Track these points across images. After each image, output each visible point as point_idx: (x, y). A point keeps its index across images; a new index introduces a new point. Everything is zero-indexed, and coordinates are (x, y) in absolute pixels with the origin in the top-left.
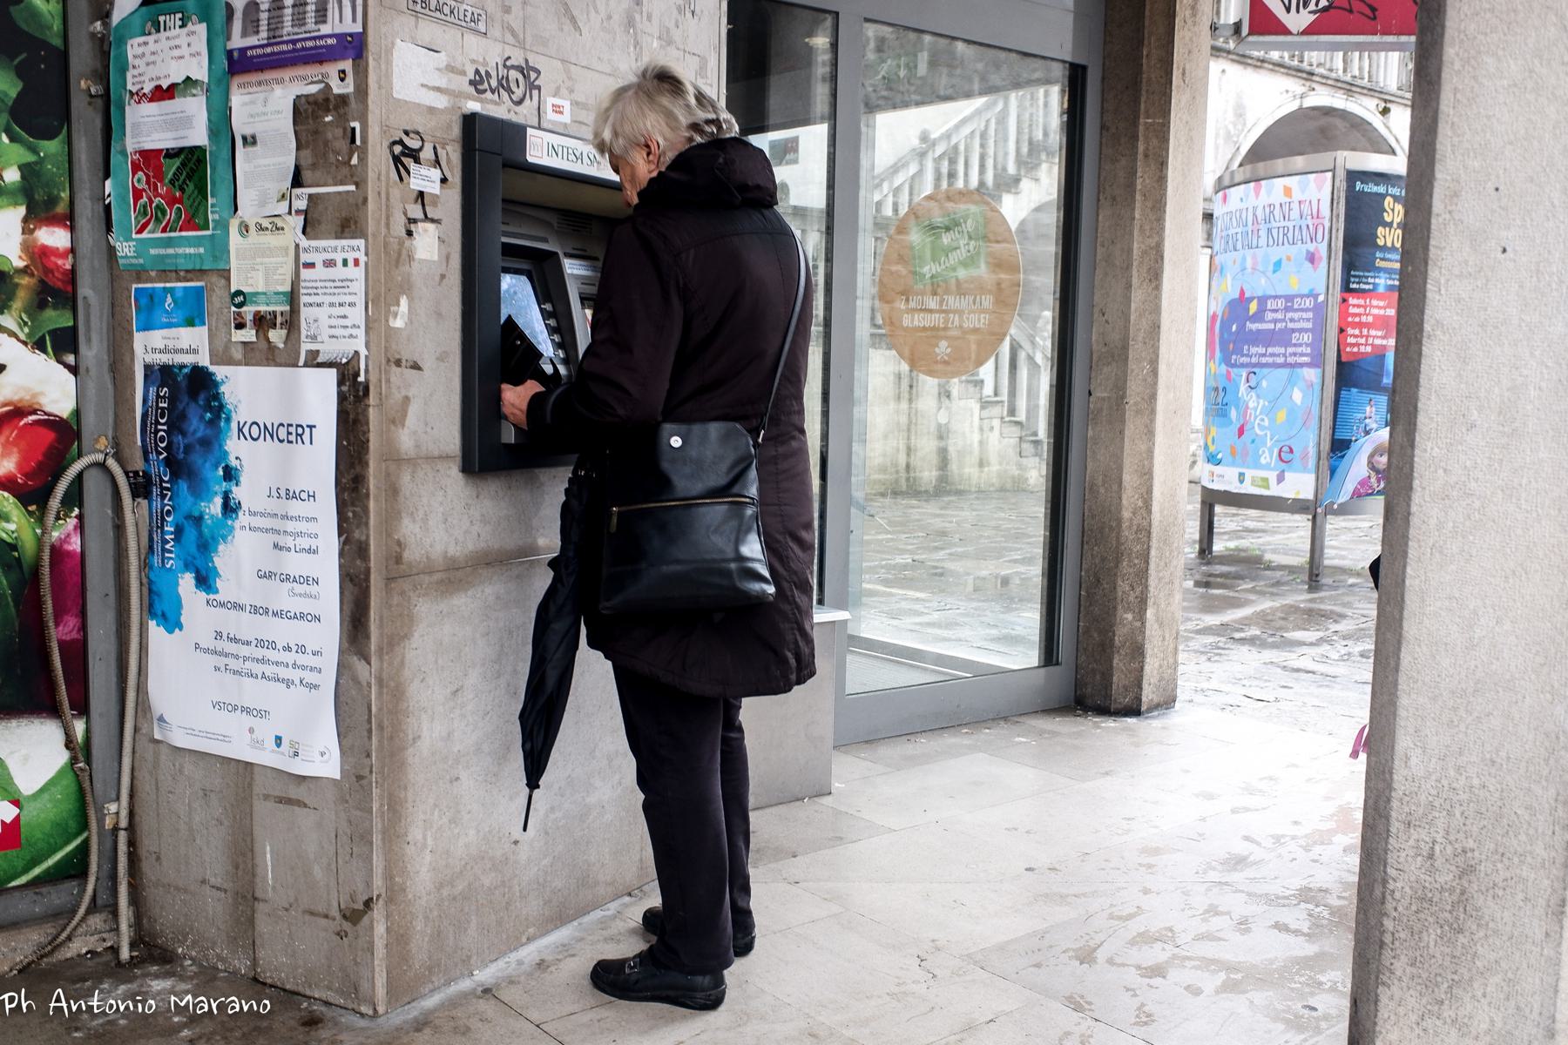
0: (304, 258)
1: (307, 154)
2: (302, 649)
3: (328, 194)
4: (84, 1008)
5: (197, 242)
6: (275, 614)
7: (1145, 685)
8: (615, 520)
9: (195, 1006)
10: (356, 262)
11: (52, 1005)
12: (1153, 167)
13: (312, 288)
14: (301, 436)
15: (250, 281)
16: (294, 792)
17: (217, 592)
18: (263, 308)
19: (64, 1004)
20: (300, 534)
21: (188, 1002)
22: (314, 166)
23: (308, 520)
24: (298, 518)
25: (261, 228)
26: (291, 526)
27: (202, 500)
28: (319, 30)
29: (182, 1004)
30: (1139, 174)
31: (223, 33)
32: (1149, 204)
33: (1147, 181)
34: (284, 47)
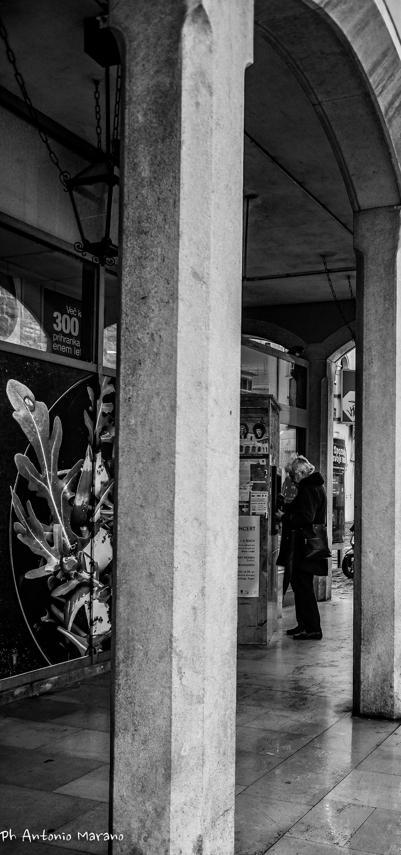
2: (249, 572)
4: (38, 838)
9: (89, 837)
10: (266, 496)
11: (24, 836)
16: (245, 601)
19: (29, 836)
20: (250, 548)
21: (86, 835)
22: (255, 477)
23: (252, 545)
26: (248, 547)
29: (83, 836)
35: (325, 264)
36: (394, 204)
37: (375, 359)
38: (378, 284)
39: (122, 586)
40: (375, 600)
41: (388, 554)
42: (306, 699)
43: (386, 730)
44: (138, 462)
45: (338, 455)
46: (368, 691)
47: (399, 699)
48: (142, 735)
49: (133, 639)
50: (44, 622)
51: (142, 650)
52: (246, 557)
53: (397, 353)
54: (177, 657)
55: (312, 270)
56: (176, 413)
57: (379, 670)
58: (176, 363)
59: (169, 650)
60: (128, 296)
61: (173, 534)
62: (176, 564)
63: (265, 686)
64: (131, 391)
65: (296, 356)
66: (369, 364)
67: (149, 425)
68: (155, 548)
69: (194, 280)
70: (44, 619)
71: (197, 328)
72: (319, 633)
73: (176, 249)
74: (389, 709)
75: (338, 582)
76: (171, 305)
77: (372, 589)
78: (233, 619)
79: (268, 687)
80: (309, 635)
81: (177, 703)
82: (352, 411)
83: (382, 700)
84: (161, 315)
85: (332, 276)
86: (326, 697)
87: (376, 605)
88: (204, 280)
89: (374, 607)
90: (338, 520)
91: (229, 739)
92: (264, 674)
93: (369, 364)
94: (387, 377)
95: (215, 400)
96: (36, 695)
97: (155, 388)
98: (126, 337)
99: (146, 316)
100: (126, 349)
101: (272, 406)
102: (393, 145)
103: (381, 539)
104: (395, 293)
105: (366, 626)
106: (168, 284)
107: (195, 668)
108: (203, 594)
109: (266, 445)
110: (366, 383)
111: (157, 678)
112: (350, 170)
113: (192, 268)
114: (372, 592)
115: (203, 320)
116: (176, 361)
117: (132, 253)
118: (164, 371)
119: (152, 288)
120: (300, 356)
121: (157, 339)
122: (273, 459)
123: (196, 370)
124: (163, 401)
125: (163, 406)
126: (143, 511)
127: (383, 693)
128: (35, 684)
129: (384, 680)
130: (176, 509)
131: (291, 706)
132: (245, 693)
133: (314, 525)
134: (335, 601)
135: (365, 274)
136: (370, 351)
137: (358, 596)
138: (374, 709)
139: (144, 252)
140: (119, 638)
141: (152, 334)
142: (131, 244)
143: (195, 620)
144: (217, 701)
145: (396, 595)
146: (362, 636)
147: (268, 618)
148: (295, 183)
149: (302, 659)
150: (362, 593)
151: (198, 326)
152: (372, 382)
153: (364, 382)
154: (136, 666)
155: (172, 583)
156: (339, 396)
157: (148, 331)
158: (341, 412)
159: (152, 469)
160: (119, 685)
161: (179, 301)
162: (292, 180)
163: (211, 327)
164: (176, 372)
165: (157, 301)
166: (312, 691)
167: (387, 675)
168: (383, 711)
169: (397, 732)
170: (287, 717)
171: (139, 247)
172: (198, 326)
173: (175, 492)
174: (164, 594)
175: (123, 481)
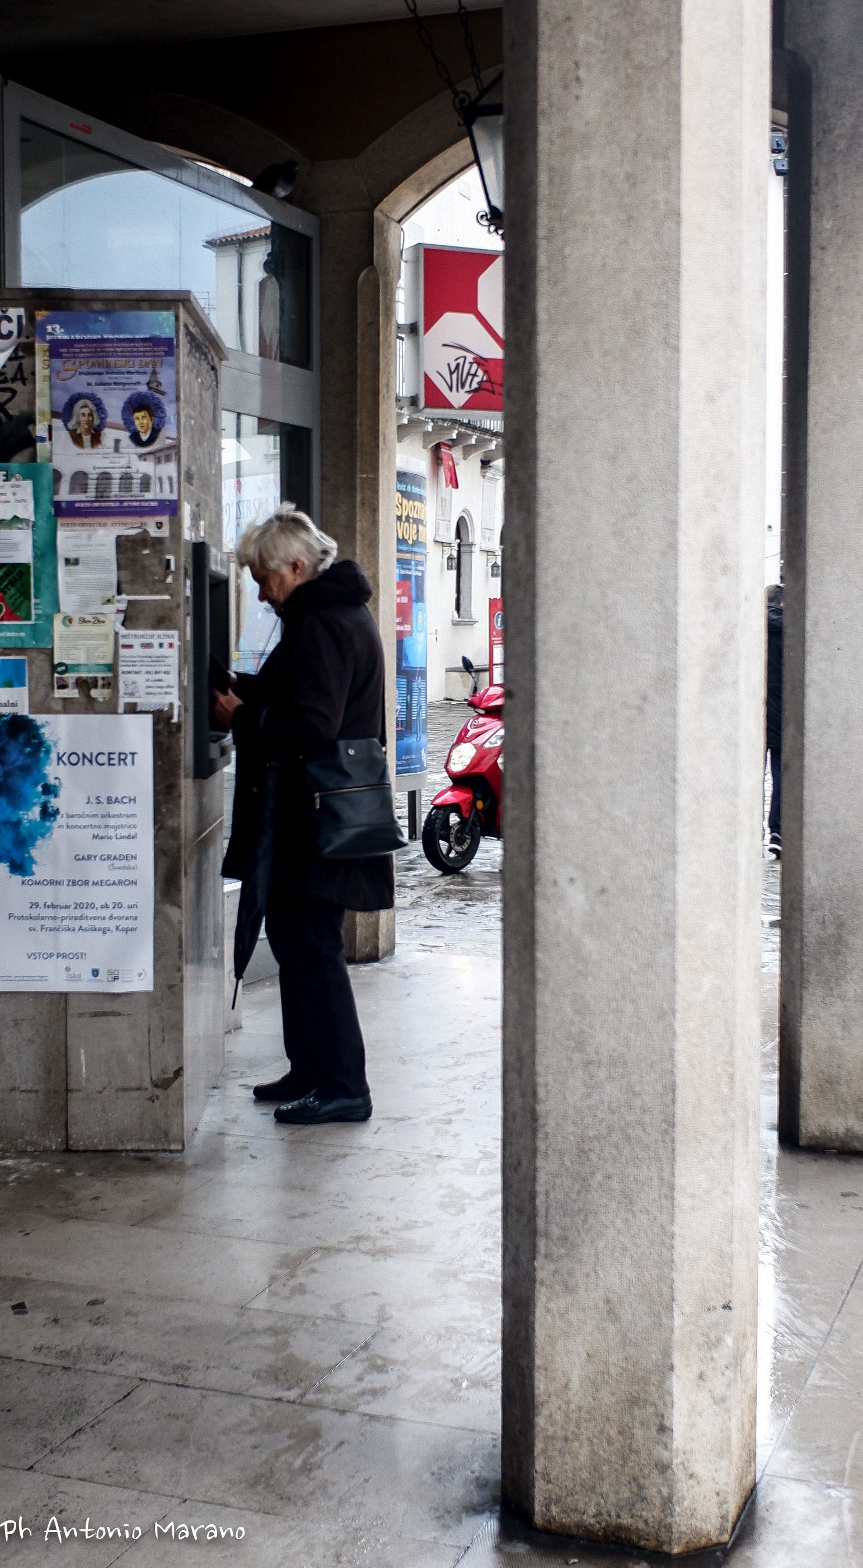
0: (122, 641)
1: (123, 573)
2: (118, 905)
3: (146, 600)
5: (20, 628)
6: (95, 884)
7: (380, 936)
8: (318, 801)
10: (171, 645)
12: (368, 512)
13: (131, 661)
14: (124, 760)
15: (72, 656)
16: (109, 1006)
17: (33, 874)
18: (84, 675)
20: (122, 826)
22: (132, 582)
23: (128, 816)
24: (120, 816)
25: (83, 621)
26: (112, 822)
27: (21, 810)
28: (143, 496)
30: (358, 518)
31: (49, 489)
32: (367, 542)
33: (365, 524)
34: (112, 504)
45: (408, 518)
46: (566, 1439)
47: (691, 1476)
52: (109, 857)
57: (613, 1359)
63: (162, 1364)
65: (276, 197)
66: (566, 87)
72: (359, 1101)
74: (652, 1514)
75: (412, 888)
77: (582, 1032)
80: (328, 1108)
82: (454, 376)
83: (624, 1479)
86: (391, 1420)
87: (596, 1097)
89: (590, 1108)
90: (409, 707)
92: (163, 1299)
93: (566, 87)
101: (189, 333)
105: (558, 1181)
109: (169, 469)
110: (551, 169)
114: (580, 1046)
120: (288, 200)
122: (196, 518)
127: (627, 1453)
129: (634, 1402)
131: (253, 1484)
133: (341, 744)
136: (570, 32)
137: (520, 1058)
138: (592, 1510)
145: (681, 1061)
146: (541, 1223)
150: (540, 1048)
152: (578, 166)
156: (413, 329)
158: (418, 377)
167: (645, 1381)
168: (626, 1520)
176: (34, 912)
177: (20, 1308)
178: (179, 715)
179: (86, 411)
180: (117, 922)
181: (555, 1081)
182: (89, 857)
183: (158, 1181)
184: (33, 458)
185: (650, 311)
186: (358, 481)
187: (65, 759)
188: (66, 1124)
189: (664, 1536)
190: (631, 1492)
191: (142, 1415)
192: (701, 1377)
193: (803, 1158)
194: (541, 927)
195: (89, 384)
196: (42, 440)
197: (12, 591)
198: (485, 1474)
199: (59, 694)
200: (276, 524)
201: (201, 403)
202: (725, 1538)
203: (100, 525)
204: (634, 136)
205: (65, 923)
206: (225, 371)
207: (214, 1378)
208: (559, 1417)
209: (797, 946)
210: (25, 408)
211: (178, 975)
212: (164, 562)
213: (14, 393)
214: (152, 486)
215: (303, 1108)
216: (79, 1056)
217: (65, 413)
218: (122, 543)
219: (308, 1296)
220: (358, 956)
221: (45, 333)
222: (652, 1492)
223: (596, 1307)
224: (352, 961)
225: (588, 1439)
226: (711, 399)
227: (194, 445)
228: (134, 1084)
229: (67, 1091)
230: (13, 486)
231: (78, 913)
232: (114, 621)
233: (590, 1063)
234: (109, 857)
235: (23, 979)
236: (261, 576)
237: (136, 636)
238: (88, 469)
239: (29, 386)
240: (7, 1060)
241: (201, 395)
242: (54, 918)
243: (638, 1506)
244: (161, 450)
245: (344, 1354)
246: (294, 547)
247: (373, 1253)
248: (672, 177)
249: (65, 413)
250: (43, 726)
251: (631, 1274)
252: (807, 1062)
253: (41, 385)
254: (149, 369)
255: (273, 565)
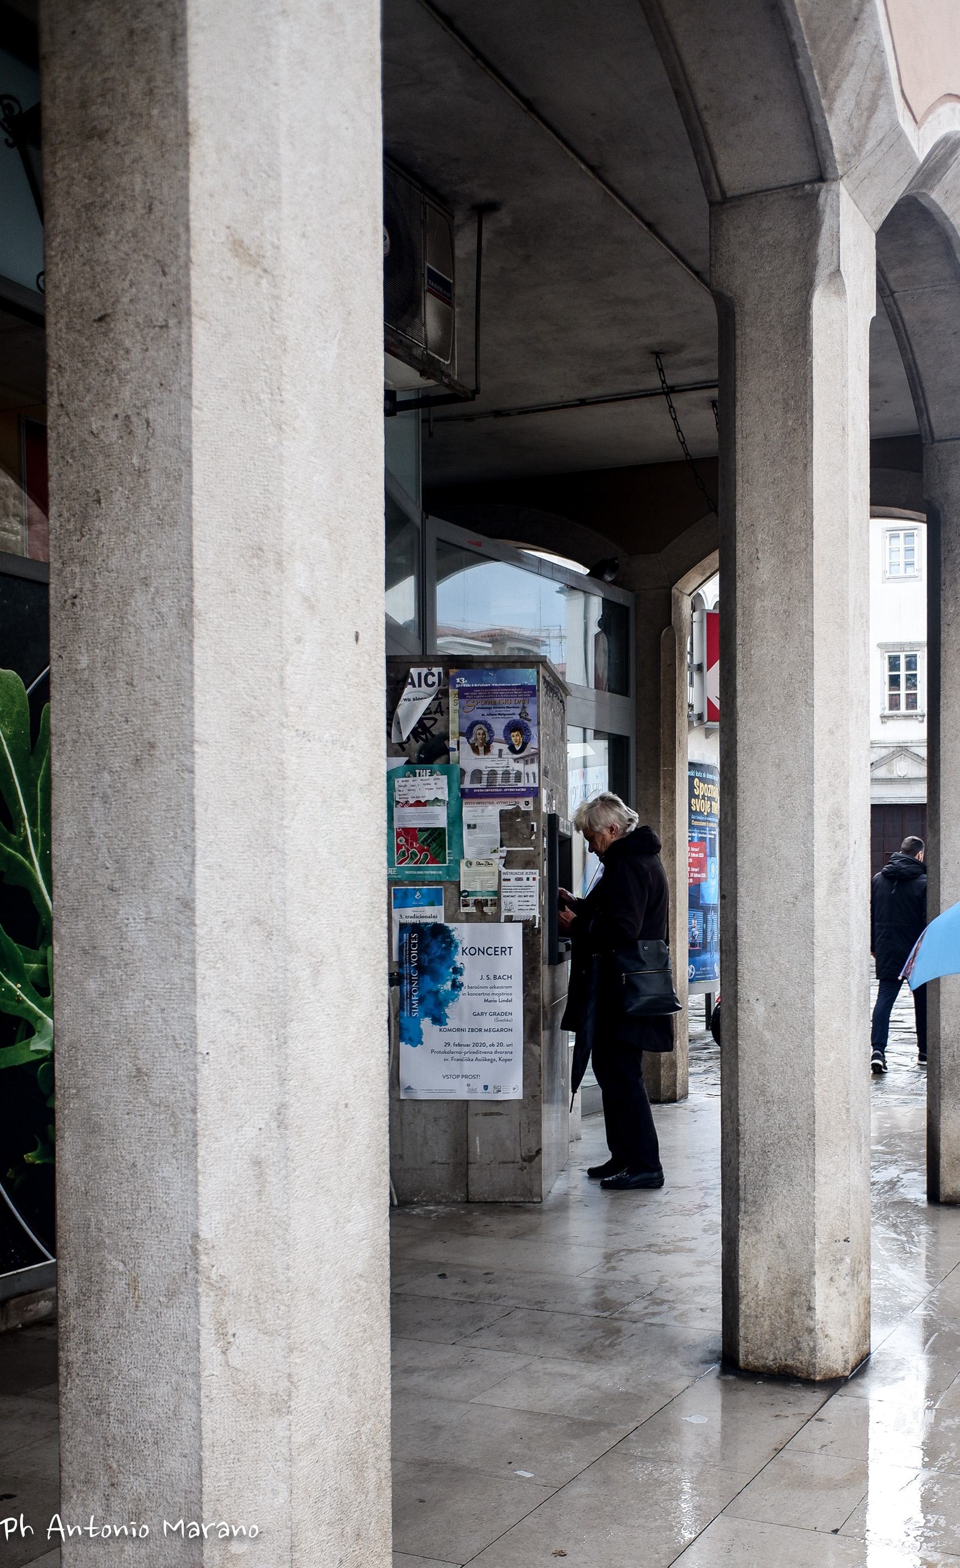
2: (501, 1044)
5: (439, 869)
10: (534, 879)
16: (495, 1109)
17: (447, 1024)
18: (480, 898)
22: (510, 839)
23: (507, 987)
24: (502, 987)
25: (479, 864)
26: (496, 991)
34: (497, 790)
35: (661, 370)
36: (804, 179)
37: (763, 551)
38: (770, 373)
39: (69, 1103)
40: (769, 1110)
41: (800, 1006)
42: (618, 1331)
43: (796, 1410)
44: (100, 769)
45: (704, 796)
46: (757, 1317)
47: (827, 1336)
48: (129, 1499)
49: (100, 1244)
50: (32, 1165)
51: (121, 1273)
52: (495, 1014)
53: (815, 535)
54: (212, 1294)
55: (635, 388)
56: (191, 632)
57: (782, 1269)
58: (191, 493)
59: (191, 1275)
60: (62, 318)
61: (193, 962)
62: (202, 1046)
64: (78, 577)
65: (604, 581)
67: (124, 667)
68: (147, 1002)
69: (236, 262)
70: (29, 1157)
71: (248, 397)
72: (656, 1174)
73: (180, 174)
74: (804, 1358)
75: (705, 1061)
76: (174, 332)
78: (378, 1186)
79: (536, 1303)
80: (635, 1179)
81: (217, 1417)
84: (148, 364)
85: (679, 401)
87: (772, 1121)
88: (266, 263)
91: (372, 1496)
94: (793, 591)
95: (306, 599)
96: (15, 1327)
97: (136, 566)
98: (61, 429)
99: (111, 368)
100: (61, 463)
101: (545, 681)
102: (801, 19)
103: (783, 970)
104: (809, 393)
106: (164, 274)
107: (263, 1322)
108: (282, 1125)
109: (533, 768)
111: (162, 1349)
112: (699, 95)
113: (228, 227)
114: (763, 1093)
115: (263, 374)
116: (191, 487)
117: (68, 193)
118: (159, 518)
119: (123, 290)
120: (613, 583)
121: (140, 431)
122: (550, 798)
123: (247, 514)
124: (158, 600)
125: (159, 613)
126: (115, 902)
127: (790, 1323)
128: (13, 1302)
129: (794, 1293)
130: (198, 895)
131: (581, 1351)
132: (481, 1318)
133: (640, 942)
134: (696, 1102)
135: (738, 351)
136: (753, 532)
137: (730, 1102)
138: (771, 1357)
139: (100, 190)
140: (66, 1242)
141: (128, 417)
142: (64, 169)
143: (260, 1193)
144: (331, 1402)
145: (818, 1099)
146: (741, 1193)
147: (545, 1141)
148: (583, 167)
149: (617, 1234)
151: (250, 392)
152: (758, 605)
153: (738, 606)
154: (109, 1314)
155: (194, 1096)
156: (700, 668)
157: (115, 411)
158: (703, 699)
159: (137, 786)
160: (68, 1365)
161: (194, 319)
162: (576, 159)
163: (286, 396)
164: (190, 518)
165: (137, 325)
166: (634, 1313)
167: (800, 1281)
168: (790, 1362)
169: (822, 1414)
170: (573, 1377)
171: (85, 177)
172: (250, 392)
173: (194, 849)
174: (175, 1126)
175: (63, 822)
176: (448, 1049)
177: (443, 1276)
178: (539, 923)
179: (481, 732)
180: (500, 1055)
181: (749, 1113)
182: (482, 1014)
183: (526, 1219)
184: (448, 761)
185: (797, 685)
186: (661, 772)
187: (467, 951)
188: (467, 1184)
189: (811, 1370)
190: (793, 1345)
191: (518, 1322)
192: (831, 1279)
193: (942, 1208)
194: (740, 1026)
195: (483, 715)
196: (454, 750)
197: (434, 845)
198: (714, 1348)
199: (463, 910)
200: (600, 802)
201: (553, 725)
202: (847, 1373)
203: (490, 803)
204: (788, 589)
205: (467, 1055)
206: (569, 700)
207: (559, 1307)
208: (752, 1304)
209: (937, 1072)
210: (443, 730)
211: (539, 1088)
212: (530, 827)
213: (436, 720)
214: (522, 779)
215: (619, 1179)
216: (475, 1141)
217: (468, 733)
218: (503, 815)
219: (617, 1272)
220: (662, 1099)
221: (456, 683)
222: (804, 1345)
223: (773, 1240)
224: (657, 1101)
225: (769, 1316)
226: (831, 732)
227: (549, 751)
228: (510, 1159)
229: (468, 1163)
230: (435, 779)
231: (475, 1049)
232: (498, 864)
233: (768, 1102)
234: (495, 1014)
235: (440, 1091)
236: (590, 835)
237: (512, 874)
238: (482, 768)
239: (445, 716)
240: (430, 1143)
241: (553, 720)
242: (460, 1053)
243: (797, 1353)
244: (528, 756)
245: (637, 1297)
246: (611, 817)
247: (659, 1253)
248: (809, 612)
249: (468, 733)
250: (453, 930)
251: (791, 1221)
252: (944, 1146)
253: (454, 716)
254: (521, 705)
255: (597, 828)
